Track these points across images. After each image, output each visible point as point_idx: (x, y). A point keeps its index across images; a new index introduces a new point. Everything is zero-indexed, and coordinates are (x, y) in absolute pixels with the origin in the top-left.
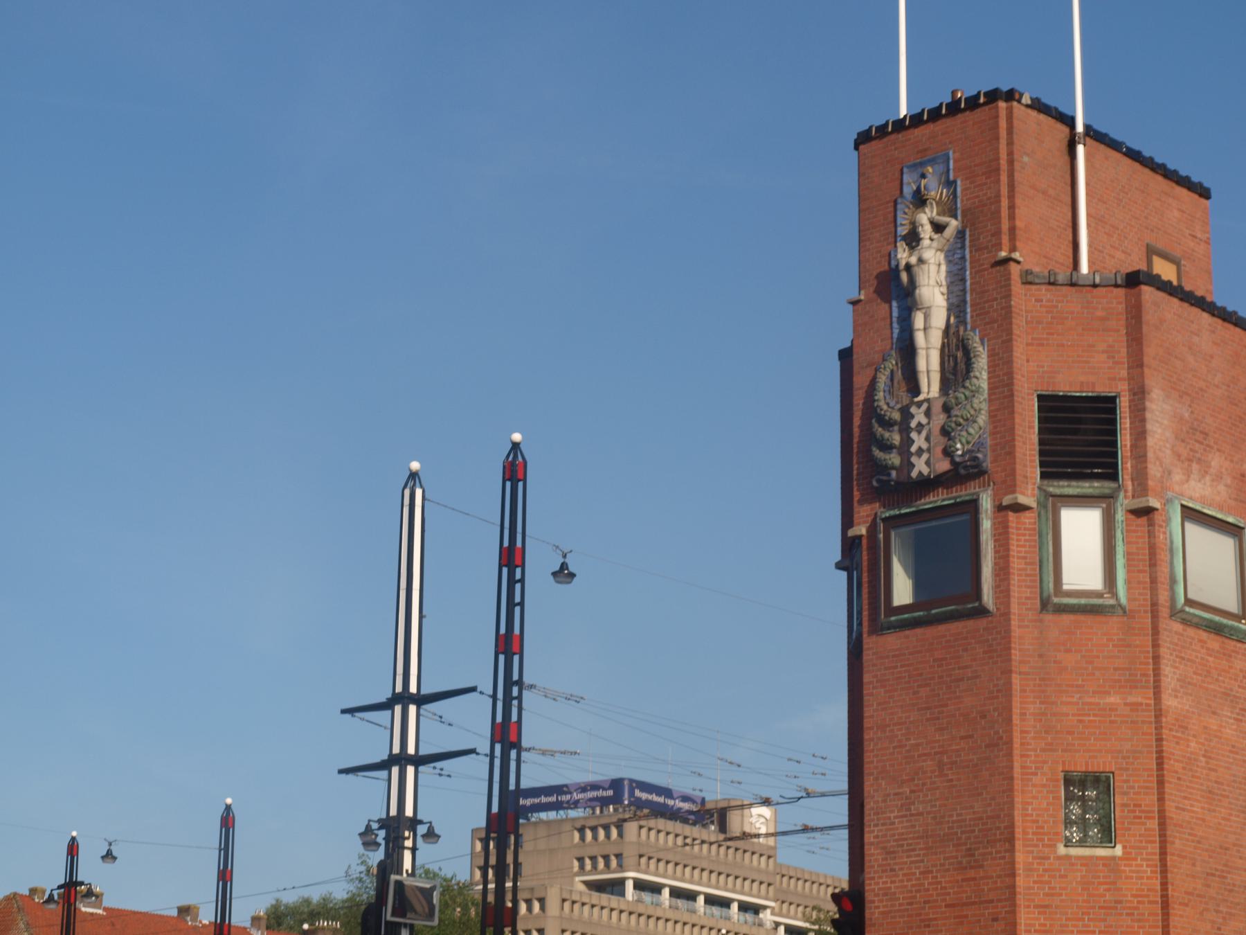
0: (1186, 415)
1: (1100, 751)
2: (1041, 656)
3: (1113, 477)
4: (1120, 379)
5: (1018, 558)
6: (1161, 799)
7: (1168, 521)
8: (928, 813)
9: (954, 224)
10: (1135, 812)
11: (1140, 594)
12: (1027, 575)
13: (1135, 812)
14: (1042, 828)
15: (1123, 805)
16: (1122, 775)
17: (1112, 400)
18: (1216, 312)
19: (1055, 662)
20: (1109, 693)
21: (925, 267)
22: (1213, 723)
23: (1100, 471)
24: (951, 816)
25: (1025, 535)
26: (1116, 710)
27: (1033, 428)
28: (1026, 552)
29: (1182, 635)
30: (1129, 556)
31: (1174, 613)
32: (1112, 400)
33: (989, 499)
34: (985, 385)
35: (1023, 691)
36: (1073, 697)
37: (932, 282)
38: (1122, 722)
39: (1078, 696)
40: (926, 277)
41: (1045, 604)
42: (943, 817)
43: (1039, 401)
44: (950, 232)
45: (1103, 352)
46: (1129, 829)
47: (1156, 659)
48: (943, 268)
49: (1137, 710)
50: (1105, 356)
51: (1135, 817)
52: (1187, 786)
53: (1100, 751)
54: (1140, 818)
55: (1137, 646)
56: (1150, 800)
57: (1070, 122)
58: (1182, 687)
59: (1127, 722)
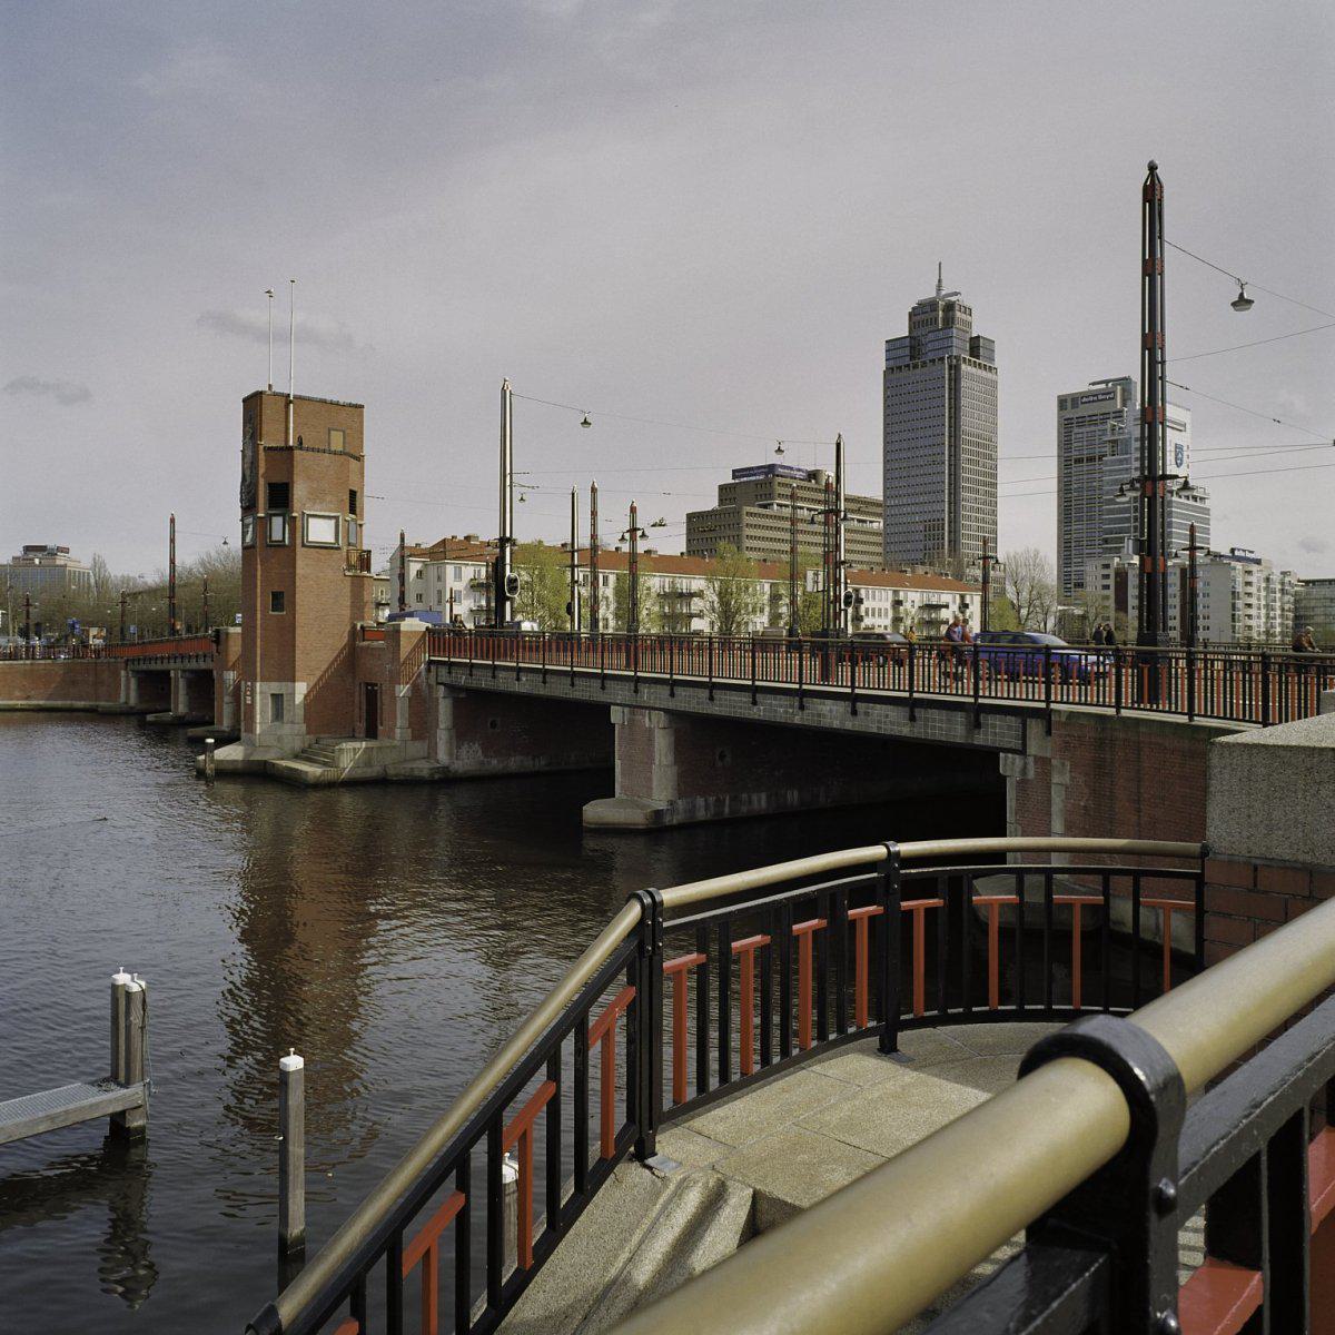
31: (303, 545)
41: (303, 545)
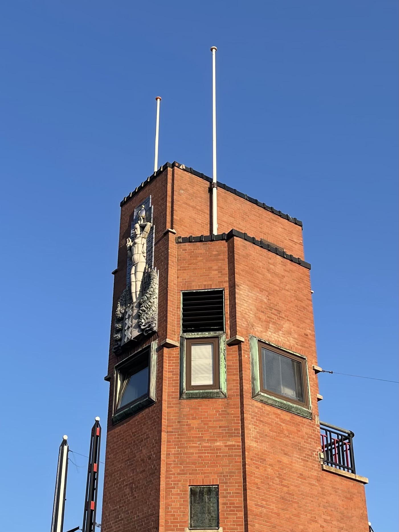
0: (265, 300)
1: (211, 473)
2: (179, 422)
3: (222, 329)
4: (225, 282)
5: (169, 372)
6: (245, 500)
7: (250, 349)
8: (126, 518)
9: (149, 225)
10: (230, 507)
11: (234, 386)
12: (173, 380)
13: (230, 507)
14: (177, 519)
15: (224, 504)
16: (223, 486)
17: (221, 292)
18: (285, 256)
19: (187, 425)
20: (216, 440)
21: (136, 246)
22: (285, 460)
23: (218, 327)
24: (134, 518)
25: (173, 360)
26: (220, 449)
27: (180, 308)
28: (173, 369)
29: (262, 409)
30: (227, 367)
32: (221, 292)
33: (156, 345)
34: (157, 291)
35: (168, 441)
36: (196, 443)
37: (140, 252)
38: (223, 456)
39: (199, 443)
40: (137, 250)
42: (131, 519)
43: (183, 296)
44: (148, 228)
45: (216, 270)
46: (227, 518)
47: (242, 420)
48: (145, 245)
49: (232, 449)
50: (217, 272)
51: (231, 511)
52: (264, 493)
53: (211, 473)
54: (234, 511)
55: (232, 414)
56: (239, 500)
57: (210, 180)
58: (261, 437)
59: (226, 456)
